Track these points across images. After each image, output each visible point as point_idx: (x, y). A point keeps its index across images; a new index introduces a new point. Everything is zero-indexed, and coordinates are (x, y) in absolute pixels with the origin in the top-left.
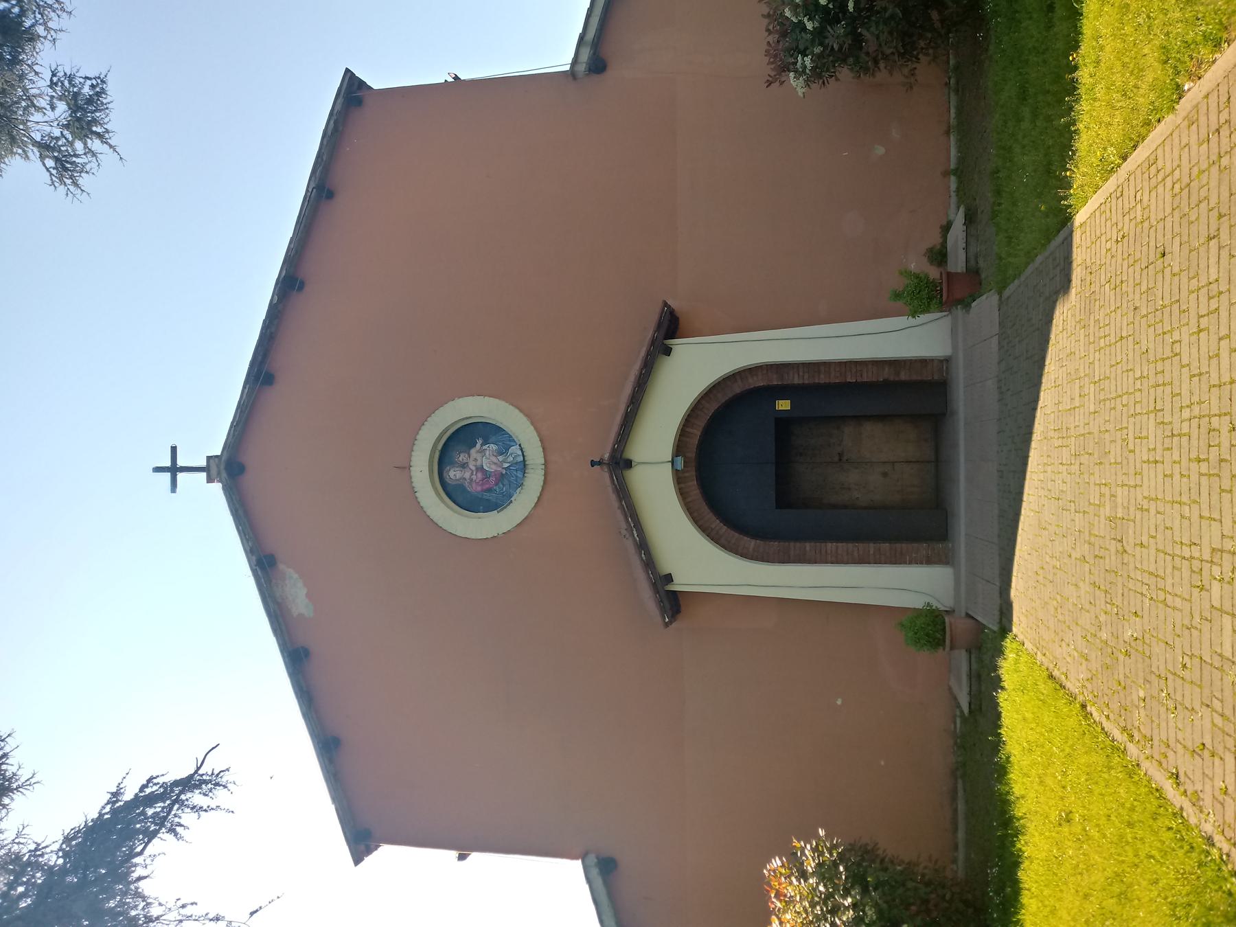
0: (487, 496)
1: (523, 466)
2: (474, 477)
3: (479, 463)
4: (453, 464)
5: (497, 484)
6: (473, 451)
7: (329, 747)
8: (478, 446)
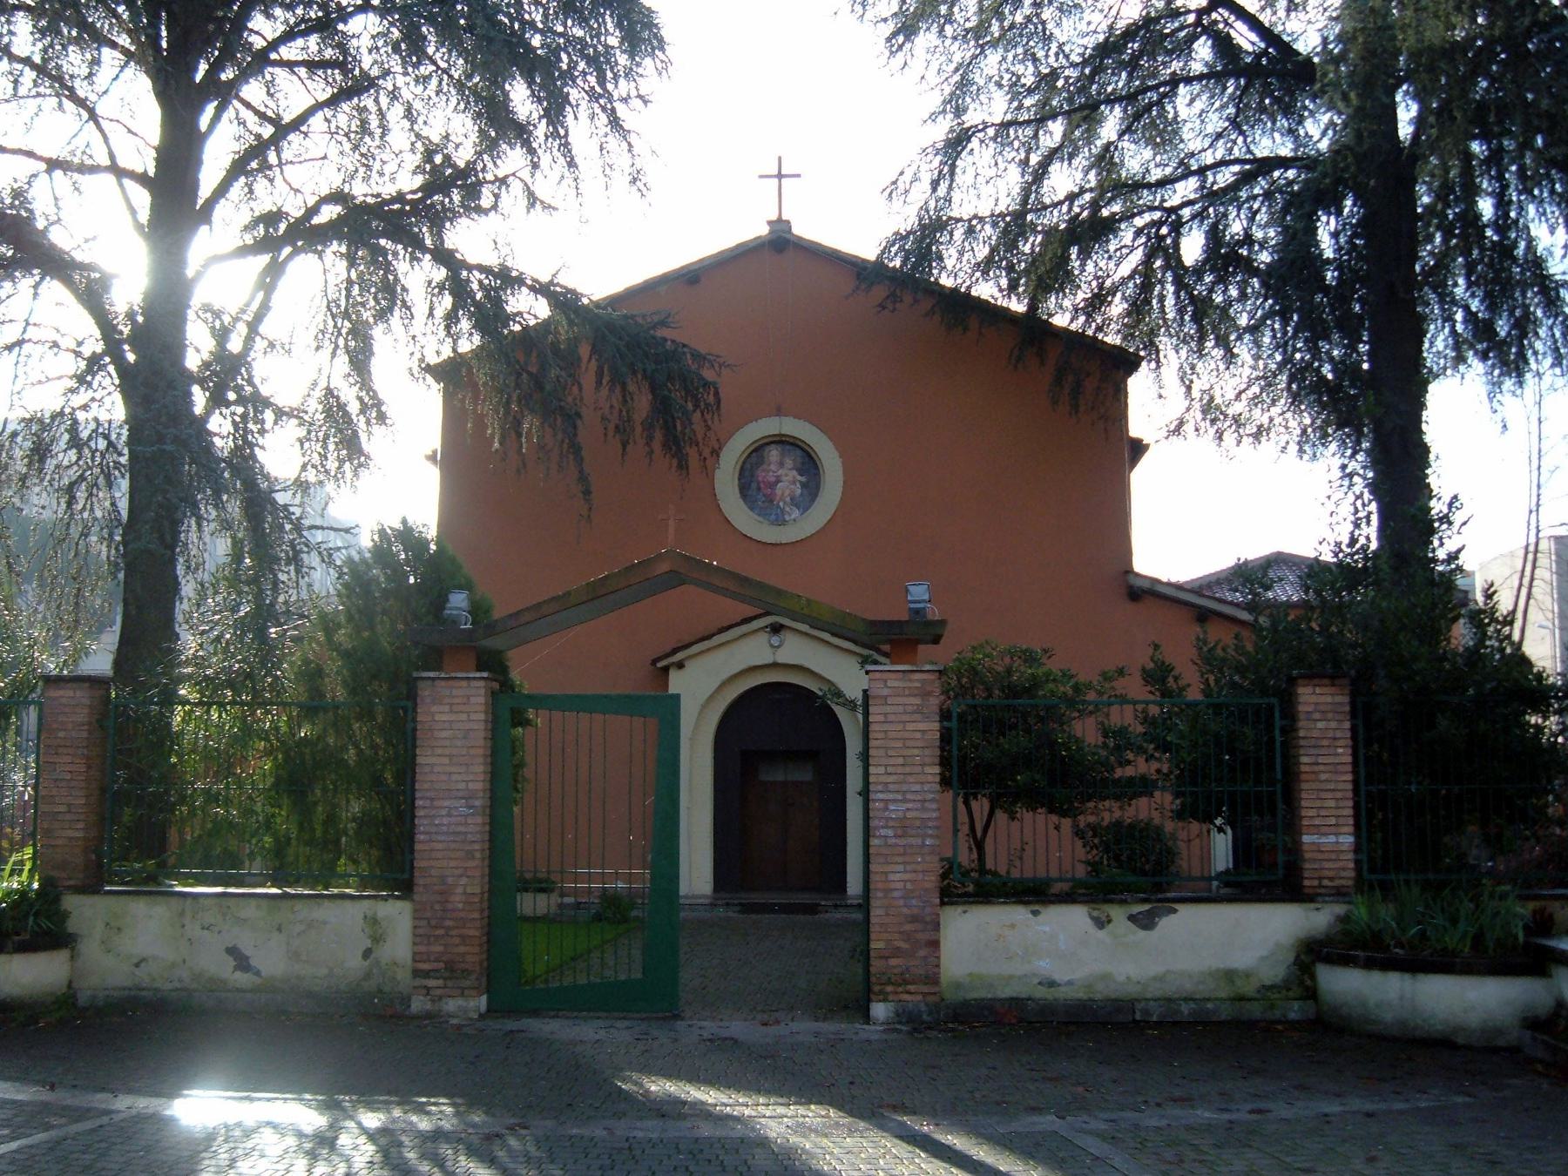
0: (754, 485)
1: (780, 521)
4: (783, 455)
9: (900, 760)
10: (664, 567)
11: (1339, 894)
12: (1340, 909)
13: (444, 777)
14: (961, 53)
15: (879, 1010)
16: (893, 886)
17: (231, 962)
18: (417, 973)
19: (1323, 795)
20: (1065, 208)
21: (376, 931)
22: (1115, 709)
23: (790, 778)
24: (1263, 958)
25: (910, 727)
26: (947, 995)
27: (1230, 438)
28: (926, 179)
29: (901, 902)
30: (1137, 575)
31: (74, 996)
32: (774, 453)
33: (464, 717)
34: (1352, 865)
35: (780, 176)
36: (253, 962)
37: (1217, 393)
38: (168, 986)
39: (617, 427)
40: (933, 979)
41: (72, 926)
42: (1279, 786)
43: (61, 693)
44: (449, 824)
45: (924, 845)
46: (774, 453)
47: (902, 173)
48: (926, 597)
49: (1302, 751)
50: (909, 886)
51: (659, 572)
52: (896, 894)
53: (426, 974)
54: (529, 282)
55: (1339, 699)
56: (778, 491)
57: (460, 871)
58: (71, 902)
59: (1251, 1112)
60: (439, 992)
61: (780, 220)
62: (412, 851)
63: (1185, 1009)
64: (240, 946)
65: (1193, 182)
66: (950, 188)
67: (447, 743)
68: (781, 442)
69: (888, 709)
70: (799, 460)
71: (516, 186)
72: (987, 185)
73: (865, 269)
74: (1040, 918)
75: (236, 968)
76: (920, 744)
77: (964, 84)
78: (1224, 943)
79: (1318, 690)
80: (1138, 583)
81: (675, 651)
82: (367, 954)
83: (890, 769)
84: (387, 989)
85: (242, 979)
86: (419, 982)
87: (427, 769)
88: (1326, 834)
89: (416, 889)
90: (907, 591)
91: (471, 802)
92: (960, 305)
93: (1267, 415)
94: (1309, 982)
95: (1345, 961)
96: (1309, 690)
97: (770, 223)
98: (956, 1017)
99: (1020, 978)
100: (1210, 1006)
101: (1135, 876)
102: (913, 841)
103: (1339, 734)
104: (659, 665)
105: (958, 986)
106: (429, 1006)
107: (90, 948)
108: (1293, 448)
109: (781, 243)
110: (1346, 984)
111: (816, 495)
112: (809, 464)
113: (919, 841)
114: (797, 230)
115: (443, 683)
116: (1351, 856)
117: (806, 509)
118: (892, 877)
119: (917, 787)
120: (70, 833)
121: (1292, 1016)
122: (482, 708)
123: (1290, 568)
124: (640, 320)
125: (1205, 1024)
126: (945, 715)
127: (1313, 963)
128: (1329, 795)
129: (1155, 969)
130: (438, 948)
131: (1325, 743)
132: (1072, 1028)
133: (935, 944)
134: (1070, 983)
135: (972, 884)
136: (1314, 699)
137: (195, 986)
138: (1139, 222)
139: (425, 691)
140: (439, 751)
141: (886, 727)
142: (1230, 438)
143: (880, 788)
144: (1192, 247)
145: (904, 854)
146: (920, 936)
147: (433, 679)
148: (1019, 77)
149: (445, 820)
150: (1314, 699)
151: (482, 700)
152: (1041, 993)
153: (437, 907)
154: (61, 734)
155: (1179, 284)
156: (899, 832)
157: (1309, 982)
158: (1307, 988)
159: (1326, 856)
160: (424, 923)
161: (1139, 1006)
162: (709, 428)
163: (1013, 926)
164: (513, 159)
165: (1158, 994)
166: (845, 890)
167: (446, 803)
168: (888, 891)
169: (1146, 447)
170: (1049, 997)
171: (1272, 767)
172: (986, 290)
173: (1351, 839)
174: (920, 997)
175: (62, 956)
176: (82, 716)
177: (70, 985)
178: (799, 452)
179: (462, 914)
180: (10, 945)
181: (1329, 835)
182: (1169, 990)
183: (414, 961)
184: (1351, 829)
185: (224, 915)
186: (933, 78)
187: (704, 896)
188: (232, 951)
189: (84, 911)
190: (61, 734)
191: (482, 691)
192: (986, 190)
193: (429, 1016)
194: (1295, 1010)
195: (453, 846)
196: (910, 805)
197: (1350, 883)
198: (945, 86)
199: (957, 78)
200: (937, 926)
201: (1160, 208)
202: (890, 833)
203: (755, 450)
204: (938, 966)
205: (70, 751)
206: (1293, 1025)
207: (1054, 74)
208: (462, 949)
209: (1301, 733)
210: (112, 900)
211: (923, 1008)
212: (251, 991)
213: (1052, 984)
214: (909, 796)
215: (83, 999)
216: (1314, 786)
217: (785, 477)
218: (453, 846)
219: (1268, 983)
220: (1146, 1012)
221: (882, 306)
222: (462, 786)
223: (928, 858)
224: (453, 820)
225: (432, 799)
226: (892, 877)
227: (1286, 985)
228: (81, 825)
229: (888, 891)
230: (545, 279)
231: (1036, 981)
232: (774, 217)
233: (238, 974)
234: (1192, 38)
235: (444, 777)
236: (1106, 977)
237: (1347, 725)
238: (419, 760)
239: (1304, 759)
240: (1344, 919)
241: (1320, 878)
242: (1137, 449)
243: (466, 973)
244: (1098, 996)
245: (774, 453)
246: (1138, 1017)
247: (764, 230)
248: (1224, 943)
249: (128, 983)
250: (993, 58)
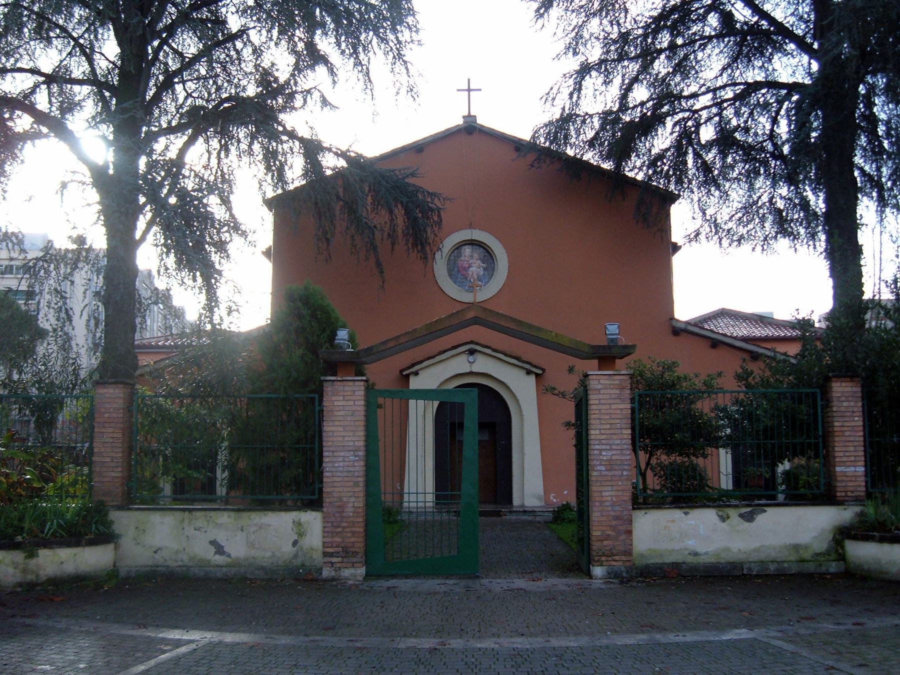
0: (456, 269)
6: (479, 262)
9: (608, 426)
10: (471, 315)
11: (857, 500)
12: (858, 509)
13: (340, 439)
14: (575, 20)
15: (598, 571)
16: (604, 499)
17: (213, 550)
18: (325, 554)
19: (847, 444)
20: (639, 109)
21: (300, 530)
22: (720, 395)
24: (815, 537)
25: (613, 407)
26: (637, 562)
27: (725, 242)
28: (566, 92)
29: (610, 508)
30: (678, 321)
31: (118, 571)
32: (468, 250)
33: (352, 403)
34: (864, 484)
35: (469, 90)
36: (226, 549)
37: (719, 217)
38: (175, 564)
39: (389, 234)
40: (628, 552)
41: (117, 528)
42: (821, 439)
43: (105, 390)
44: (343, 467)
45: (622, 475)
46: (468, 250)
47: (552, 89)
48: (617, 332)
49: (835, 419)
50: (614, 499)
51: (469, 317)
52: (607, 504)
53: (331, 555)
54: (334, 150)
55: (854, 389)
57: (352, 494)
58: (114, 515)
59: (854, 624)
60: (338, 565)
61: (469, 116)
62: (321, 482)
63: (772, 567)
64: (218, 540)
65: (710, 95)
66: (579, 98)
67: (342, 418)
68: (472, 244)
69: (601, 396)
70: (482, 255)
71: (316, 95)
72: (600, 97)
73: (523, 145)
74: (689, 516)
75: (216, 553)
76: (620, 417)
77: (578, 37)
78: (793, 529)
79: (844, 384)
80: (678, 325)
81: (413, 365)
82: (295, 543)
83: (602, 432)
84: (307, 564)
85: (219, 559)
86: (327, 559)
87: (331, 434)
88: (849, 466)
89: (324, 505)
90: (606, 328)
91: (356, 453)
92: (578, 165)
93: (746, 229)
94: (841, 551)
95: (866, 538)
96: (838, 384)
97: (464, 117)
98: (641, 575)
99: (677, 551)
100: (786, 565)
101: (753, 492)
102: (616, 473)
103: (855, 409)
105: (642, 556)
106: (333, 574)
107: (127, 542)
108: (759, 248)
109: (470, 128)
110: (864, 552)
111: (492, 275)
112: (488, 255)
113: (620, 472)
114: (480, 121)
115: (339, 383)
116: (863, 478)
118: (604, 494)
119: (618, 442)
120: (113, 474)
121: (832, 570)
122: (363, 398)
123: (730, 317)
124: (397, 173)
125: (785, 575)
126: (632, 400)
127: (843, 539)
128: (850, 444)
129: (757, 544)
130: (338, 539)
131: (848, 414)
132: (710, 579)
133: (630, 532)
134: (706, 553)
135: (642, 500)
136: (841, 389)
137: (191, 564)
138: (677, 117)
139: (328, 389)
140: (337, 423)
141: (601, 407)
142: (725, 242)
143: (597, 442)
144: (707, 133)
145: (612, 480)
146: (621, 528)
147: (333, 381)
148: (609, 34)
149: (341, 464)
150: (841, 389)
151: (362, 393)
152: (690, 559)
153: (337, 515)
154: (106, 415)
155: (697, 155)
156: (609, 468)
157: (841, 551)
158: (840, 554)
159: (849, 479)
160: (330, 524)
161: (745, 566)
162: (436, 235)
163: (673, 521)
164: (318, 77)
165: (756, 559)
166: (508, 498)
167: (342, 454)
168: (602, 502)
169: (680, 247)
170: (695, 562)
171: (816, 428)
172: (591, 157)
173: (863, 469)
174: (621, 563)
175: (111, 547)
176: (120, 404)
177: (114, 566)
179: (351, 519)
180: (84, 542)
181: (850, 467)
182: (762, 556)
183: (324, 547)
184: (862, 463)
185: (208, 521)
186: (560, 34)
188: (213, 543)
189: (124, 521)
190: (106, 415)
191: (363, 388)
192: (600, 98)
193: (333, 579)
194: (834, 567)
195: (345, 479)
196: (614, 452)
197: (863, 494)
198: (567, 38)
199: (574, 34)
200: (630, 522)
201: (689, 110)
202: (603, 468)
203: (457, 249)
204: (631, 545)
205: (112, 425)
206: (835, 575)
207: (628, 33)
208: (353, 540)
209: (835, 409)
210: (137, 513)
211: (623, 569)
212: (225, 566)
213: (696, 554)
214: (614, 447)
215: (122, 573)
216: (843, 439)
218: (345, 479)
219: (818, 551)
220: (749, 569)
221: (532, 166)
222: (351, 444)
223: (625, 483)
224: (346, 464)
225: (333, 452)
226: (604, 494)
227: (828, 553)
228: (119, 469)
229: (602, 502)
230: (344, 149)
231: (687, 552)
232: (466, 114)
233: (217, 557)
234: (707, 12)
235: (340, 439)
236: (727, 549)
237: (860, 404)
238: (325, 429)
239: (836, 424)
240: (862, 514)
241: (846, 492)
242: (676, 248)
243: (355, 554)
244: (723, 561)
245: (467, 250)
246: (745, 572)
247: (460, 122)
248: (793, 529)
249: (150, 563)
250: (595, 21)
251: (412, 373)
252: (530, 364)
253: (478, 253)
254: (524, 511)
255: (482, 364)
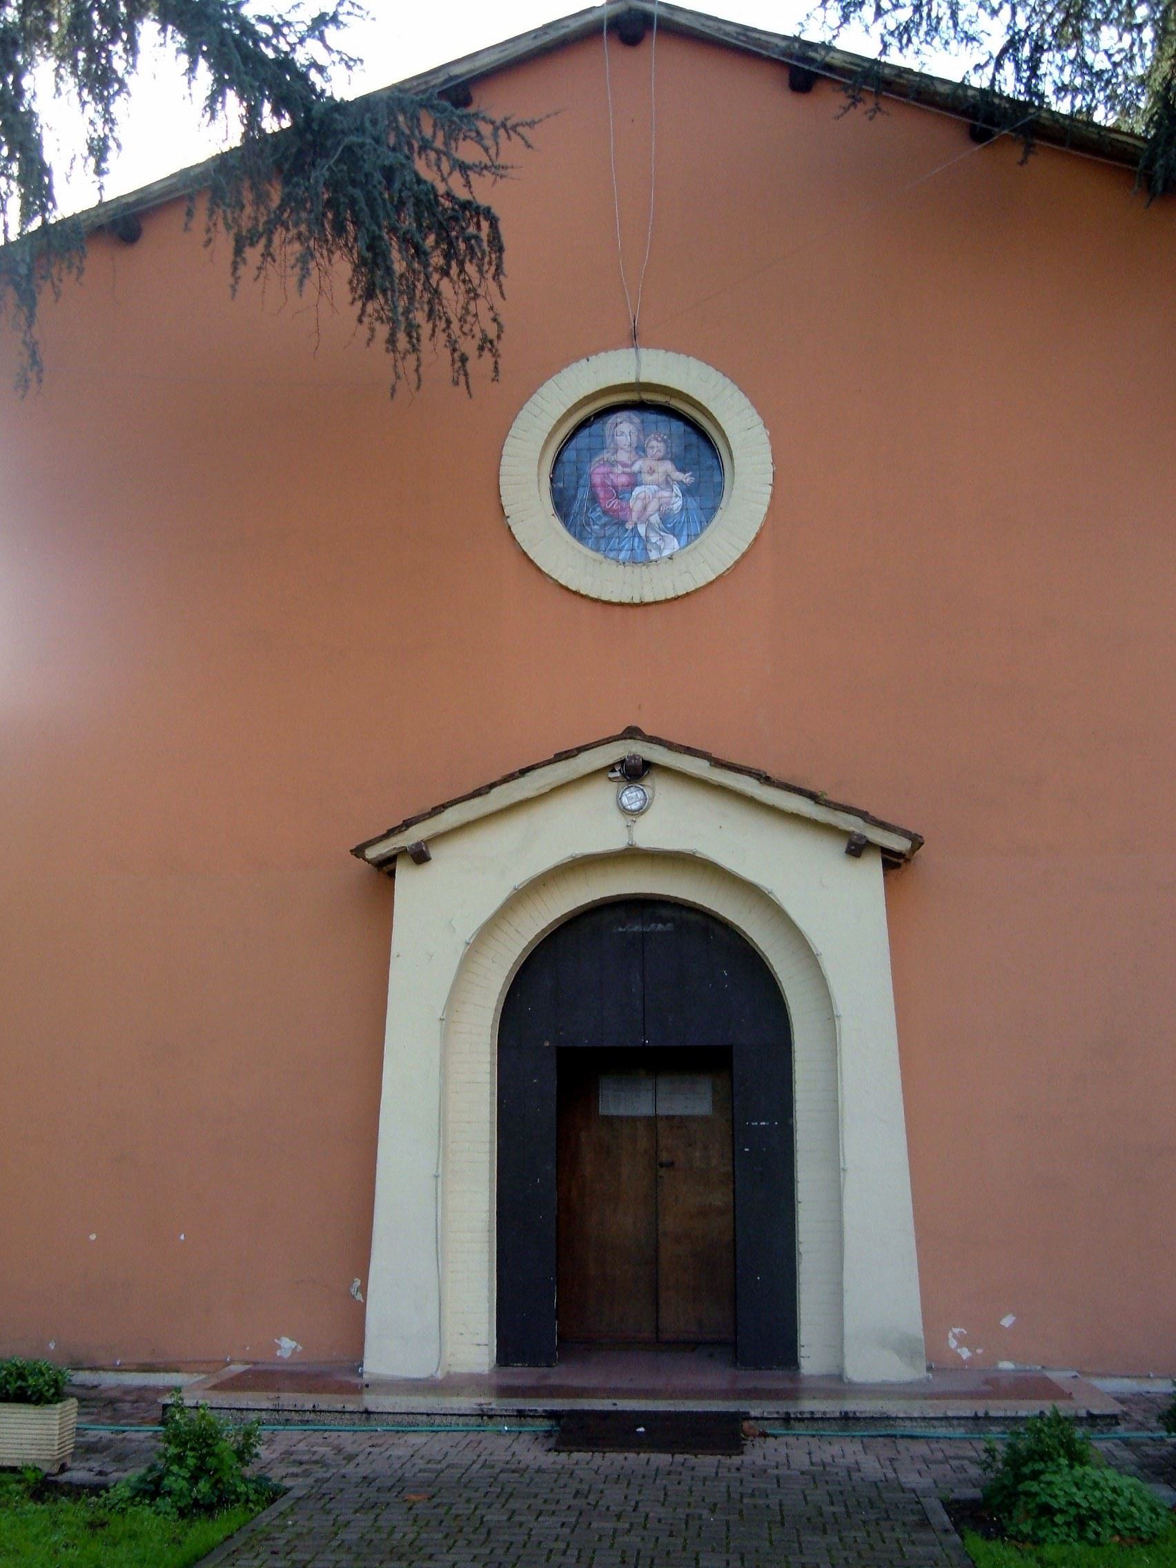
0: (583, 494)
1: (640, 558)
2: (619, 469)
3: (647, 478)
4: (644, 430)
5: (605, 512)
6: (668, 466)
7: (898, 1009)
8: (679, 476)
23: (662, 1111)
56: (636, 505)
68: (640, 406)
104: (371, 853)
111: (714, 510)
117: (693, 537)
166: (782, 1349)
178: (678, 427)
187: (470, 1383)
203: (584, 424)
217: (641, 465)
245: (624, 428)
251: (403, 852)
252: (863, 815)
253: (662, 437)
254: (847, 1419)
255: (675, 819)
